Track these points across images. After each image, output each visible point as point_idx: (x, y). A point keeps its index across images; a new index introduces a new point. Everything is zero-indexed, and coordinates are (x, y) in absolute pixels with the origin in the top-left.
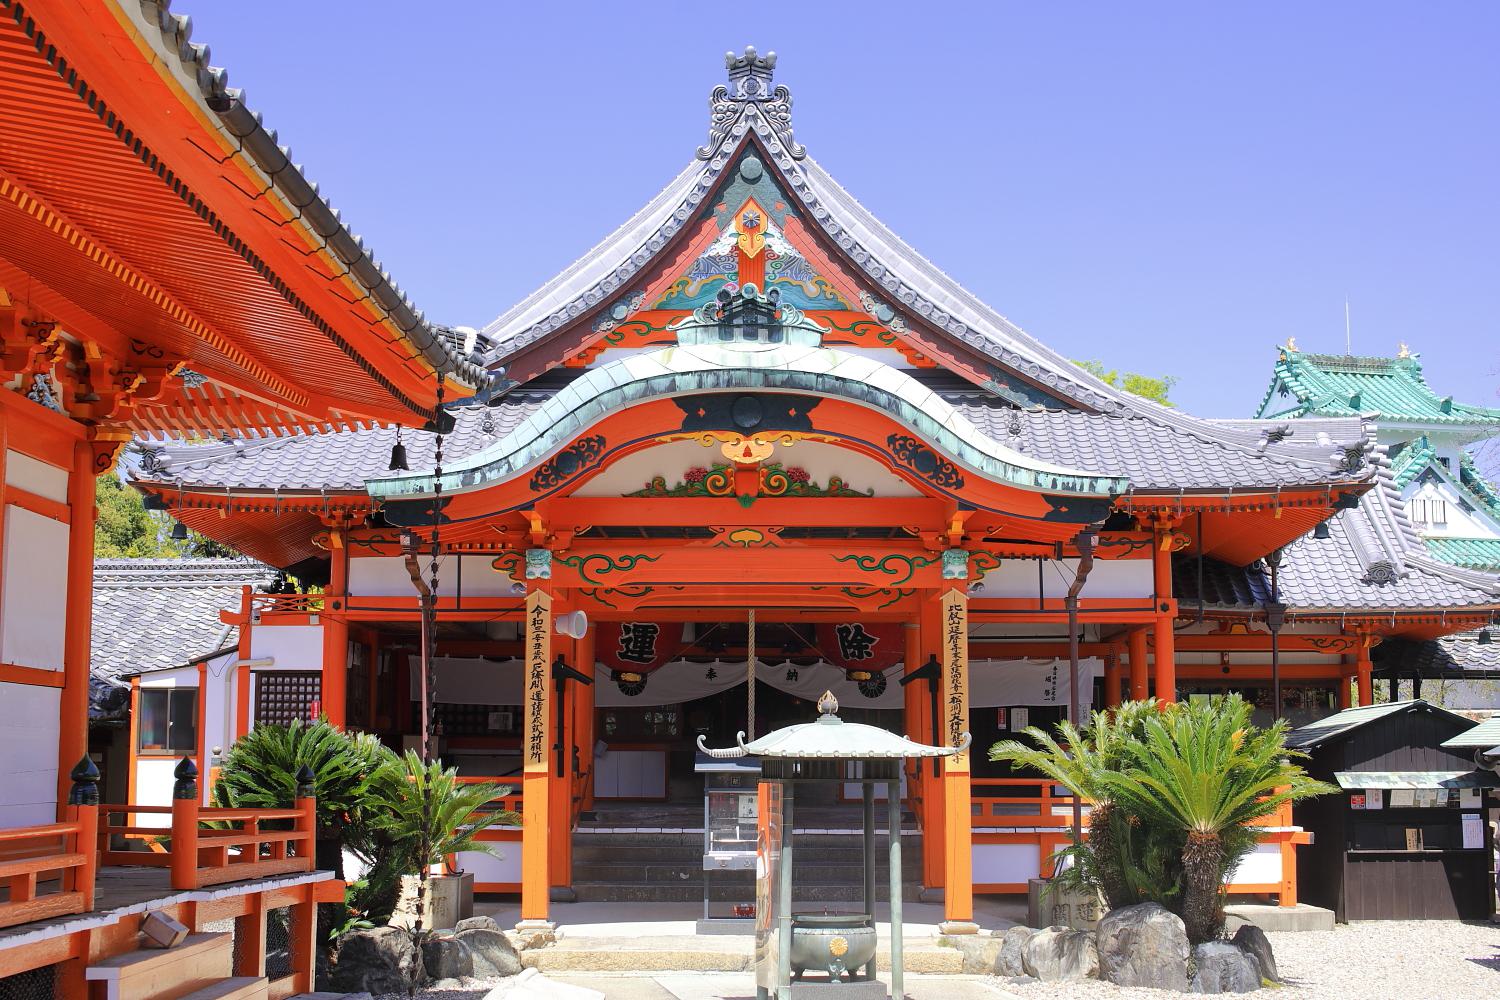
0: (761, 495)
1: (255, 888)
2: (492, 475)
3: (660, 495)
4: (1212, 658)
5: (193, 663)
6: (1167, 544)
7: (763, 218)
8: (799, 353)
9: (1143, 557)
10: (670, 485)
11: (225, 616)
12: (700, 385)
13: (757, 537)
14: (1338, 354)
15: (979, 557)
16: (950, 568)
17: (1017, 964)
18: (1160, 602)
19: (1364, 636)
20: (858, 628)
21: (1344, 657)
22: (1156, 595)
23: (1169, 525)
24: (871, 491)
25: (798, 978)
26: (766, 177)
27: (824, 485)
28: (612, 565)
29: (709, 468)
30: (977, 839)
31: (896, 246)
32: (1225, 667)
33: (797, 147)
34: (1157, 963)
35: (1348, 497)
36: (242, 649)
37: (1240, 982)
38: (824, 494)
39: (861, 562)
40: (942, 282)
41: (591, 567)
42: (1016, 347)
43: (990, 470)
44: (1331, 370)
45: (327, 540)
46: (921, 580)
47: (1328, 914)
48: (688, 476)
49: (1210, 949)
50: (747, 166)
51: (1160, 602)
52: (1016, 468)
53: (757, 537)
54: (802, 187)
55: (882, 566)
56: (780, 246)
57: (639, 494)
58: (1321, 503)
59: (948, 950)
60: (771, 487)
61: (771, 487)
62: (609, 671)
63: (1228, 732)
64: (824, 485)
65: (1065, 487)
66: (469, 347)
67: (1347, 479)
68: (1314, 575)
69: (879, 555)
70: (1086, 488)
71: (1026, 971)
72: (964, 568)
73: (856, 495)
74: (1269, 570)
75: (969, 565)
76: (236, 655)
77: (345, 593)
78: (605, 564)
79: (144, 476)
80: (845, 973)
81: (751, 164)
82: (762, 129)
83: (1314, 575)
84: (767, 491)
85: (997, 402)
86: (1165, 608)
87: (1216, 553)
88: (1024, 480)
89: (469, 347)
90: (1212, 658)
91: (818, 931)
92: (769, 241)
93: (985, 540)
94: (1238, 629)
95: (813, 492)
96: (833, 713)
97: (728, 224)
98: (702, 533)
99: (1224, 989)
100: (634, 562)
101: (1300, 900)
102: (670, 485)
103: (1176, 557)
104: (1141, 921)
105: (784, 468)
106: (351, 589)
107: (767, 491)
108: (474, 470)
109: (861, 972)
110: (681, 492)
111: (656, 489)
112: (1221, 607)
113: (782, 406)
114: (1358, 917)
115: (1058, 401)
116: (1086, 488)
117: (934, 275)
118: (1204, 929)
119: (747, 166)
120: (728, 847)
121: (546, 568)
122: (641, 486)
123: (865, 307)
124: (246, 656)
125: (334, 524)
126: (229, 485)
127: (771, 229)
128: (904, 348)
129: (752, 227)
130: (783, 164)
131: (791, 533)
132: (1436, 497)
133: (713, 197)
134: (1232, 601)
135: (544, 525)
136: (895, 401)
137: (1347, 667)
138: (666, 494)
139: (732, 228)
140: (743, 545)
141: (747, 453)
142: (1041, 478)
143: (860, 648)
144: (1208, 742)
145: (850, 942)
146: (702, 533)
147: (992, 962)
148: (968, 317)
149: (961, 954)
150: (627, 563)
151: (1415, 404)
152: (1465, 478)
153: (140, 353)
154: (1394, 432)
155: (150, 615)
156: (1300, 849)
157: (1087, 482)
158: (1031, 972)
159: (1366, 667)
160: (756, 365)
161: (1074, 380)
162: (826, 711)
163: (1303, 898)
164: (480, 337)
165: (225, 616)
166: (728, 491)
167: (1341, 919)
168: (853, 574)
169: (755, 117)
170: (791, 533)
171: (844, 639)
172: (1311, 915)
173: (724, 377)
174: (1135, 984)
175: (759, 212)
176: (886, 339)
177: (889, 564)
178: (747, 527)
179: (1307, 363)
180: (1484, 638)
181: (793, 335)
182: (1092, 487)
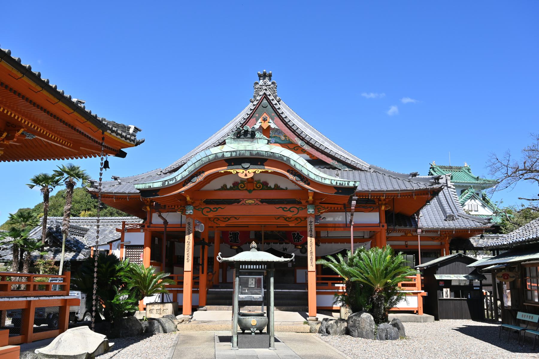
0: (254, 190)
1: (29, 299)
2: (171, 182)
3: (225, 190)
4: (403, 243)
5: (108, 243)
6: (383, 208)
7: (268, 118)
8: (261, 146)
9: (376, 211)
10: (228, 187)
11: (118, 230)
12: (231, 155)
13: (253, 202)
14: (447, 165)
15: (318, 207)
16: (309, 210)
17: (325, 330)
18: (381, 225)
19: (446, 236)
20: (298, 233)
21: (441, 243)
22: (380, 222)
23: (384, 202)
24: (286, 188)
25: (243, 333)
26: (269, 106)
27: (273, 187)
28: (211, 210)
29: (240, 182)
30: (318, 293)
31: (306, 126)
32: (407, 246)
33: (278, 98)
34: (365, 330)
35: (435, 193)
36: (122, 239)
37: (391, 336)
38: (273, 189)
39: (283, 209)
40: (319, 135)
41: (205, 211)
42: (340, 153)
43: (317, 179)
44: (445, 170)
45: (146, 208)
46: (301, 214)
47: (433, 317)
48: (233, 184)
49: (382, 326)
50: (266, 105)
51: (381, 225)
52: (325, 179)
53: (253, 202)
54: (279, 109)
55: (289, 210)
56: (273, 126)
57: (219, 190)
58: (430, 194)
59: (306, 325)
60: (257, 187)
61: (257, 187)
62: (229, 246)
63: (386, 256)
64: (273, 187)
65: (340, 184)
66: (131, 131)
67: (436, 186)
68: (429, 218)
69: (288, 207)
70: (346, 185)
71: (327, 332)
72: (313, 210)
73: (282, 189)
74: (416, 217)
75: (315, 209)
76: (120, 241)
77: (151, 223)
78: (209, 210)
79: (91, 189)
80: (258, 331)
81: (265, 101)
82: (268, 93)
83: (429, 218)
84: (256, 188)
85: (334, 168)
86: (383, 226)
87: (398, 210)
88: (328, 182)
89: (131, 131)
90: (403, 243)
91: (247, 317)
92: (269, 124)
93: (320, 203)
94: (409, 235)
95: (270, 188)
96: (255, 248)
97: (258, 119)
98: (237, 201)
99: (387, 339)
100: (217, 209)
101: (424, 313)
102: (228, 187)
103: (387, 212)
104: (359, 316)
105: (261, 182)
106: (153, 222)
107: (256, 188)
108: (166, 181)
109: (265, 330)
110: (231, 188)
111: (224, 188)
112: (402, 228)
113: (257, 160)
114: (443, 318)
115: (353, 168)
116: (346, 185)
117: (317, 134)
118: (380, 318)
119: (266, 105)
120: (245, 294)
121: (191, 211)
122: (220, 187)
123: (295, 141)
124: (123, 241)
125: (148, 204)
126: (114, 192)
127: (271, 121)
128: (309, 154)
129: (265, 120)
130: (274, 102)
131: (263, 201)
132: (475, 203)
133: (254, 111)
134: (406, 226)
135: (190, 199)
136: (289, 159)
137: (442, 246)
138: (227, 189)
139: (260, 121)
140: (250, 204)
141: (246, 175)
142: (333, 182)
143: (299, 239)
144: (380, 260)
145: (257, 321)
146: (237, 201)
147: (318, 329)
148: (326, 144)
149: (309, 327)
150: (215, 209)
151: (469, 178)
152: (484, 199)
153: (9, 126)
154: (463, 186)
155: (107, 232)
156: (423, 297)
157: (347, 183)
158: (328, 333)
159: (448, 246)
160: (247, 149)
161: (351, 159)
162: (252, 248)
163: (425, 312)
164: (135, 128)
165: (118, 230)
166: (245, 188)
167: (437, 319)
168: (280, 212)
169: (266, 90)
170: (263, 201)
171: (294, 237)
172: (427, 317)
173: (238, 153)
174: (358, 337)
175: (267, 116)
176: (303, 151)
177: (292, 210)
178: (250, 199)
179: (438, 168)
180: (482, 237)
181: (259, 141)
182: (348, 184)
